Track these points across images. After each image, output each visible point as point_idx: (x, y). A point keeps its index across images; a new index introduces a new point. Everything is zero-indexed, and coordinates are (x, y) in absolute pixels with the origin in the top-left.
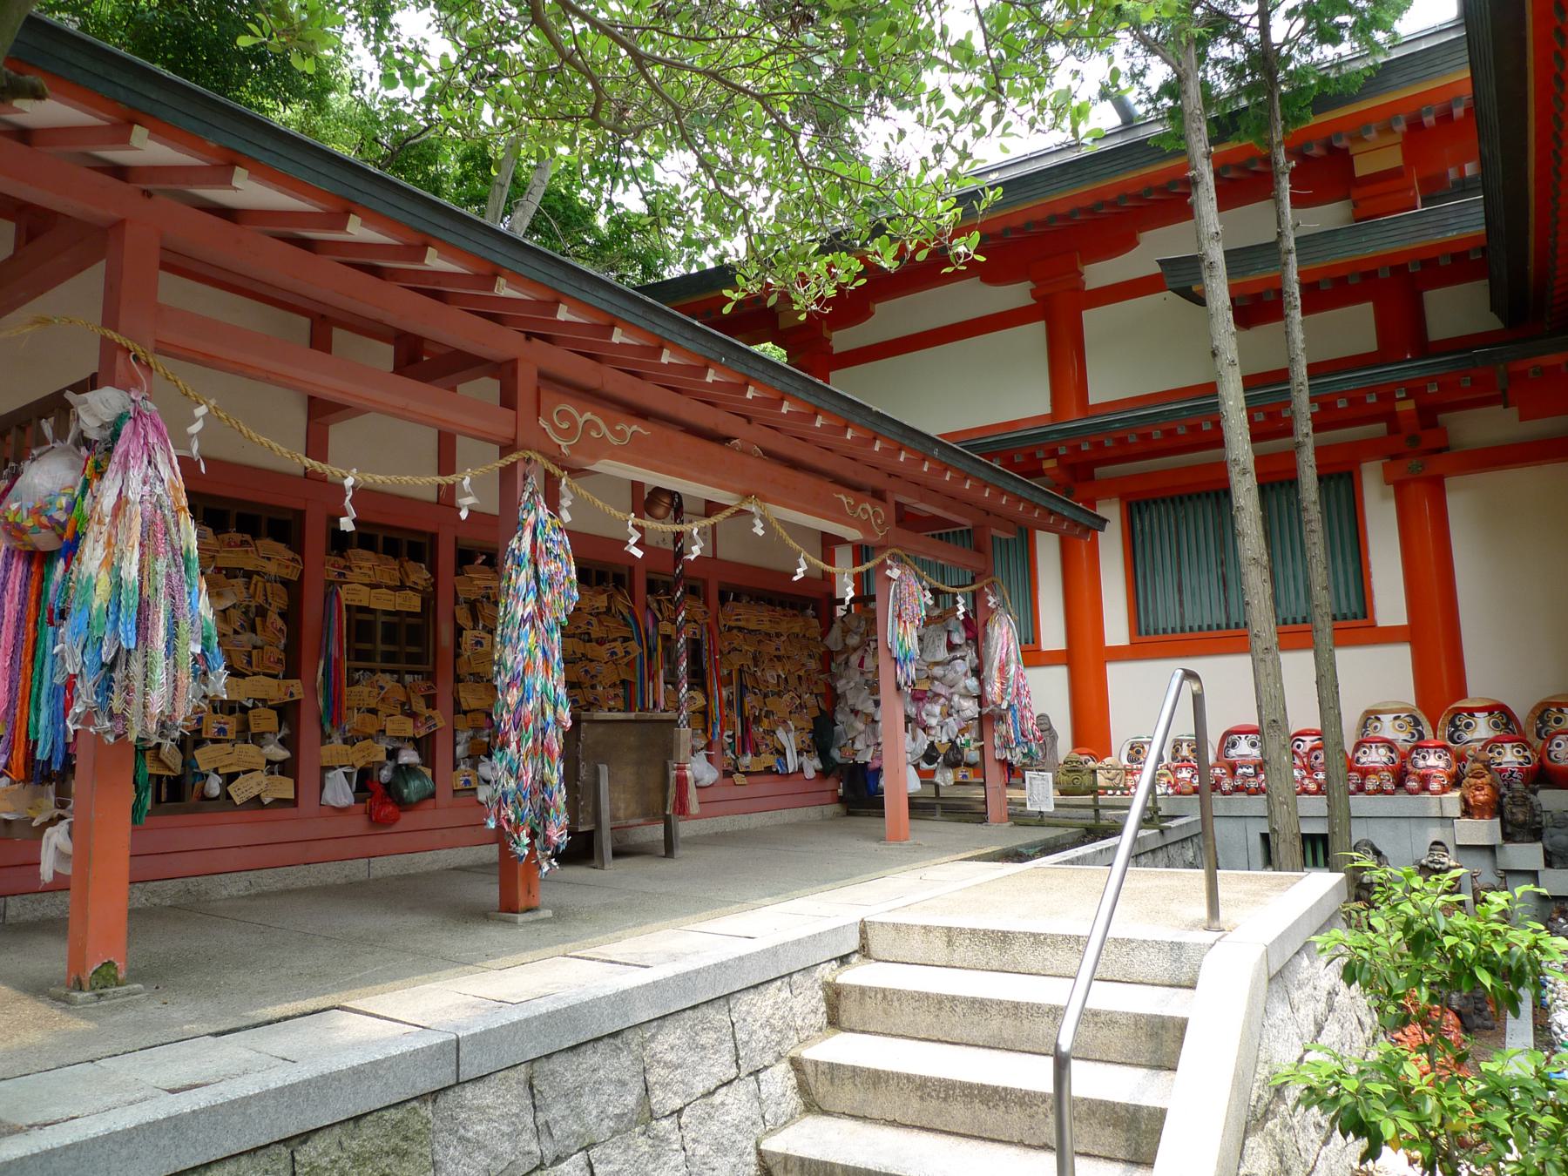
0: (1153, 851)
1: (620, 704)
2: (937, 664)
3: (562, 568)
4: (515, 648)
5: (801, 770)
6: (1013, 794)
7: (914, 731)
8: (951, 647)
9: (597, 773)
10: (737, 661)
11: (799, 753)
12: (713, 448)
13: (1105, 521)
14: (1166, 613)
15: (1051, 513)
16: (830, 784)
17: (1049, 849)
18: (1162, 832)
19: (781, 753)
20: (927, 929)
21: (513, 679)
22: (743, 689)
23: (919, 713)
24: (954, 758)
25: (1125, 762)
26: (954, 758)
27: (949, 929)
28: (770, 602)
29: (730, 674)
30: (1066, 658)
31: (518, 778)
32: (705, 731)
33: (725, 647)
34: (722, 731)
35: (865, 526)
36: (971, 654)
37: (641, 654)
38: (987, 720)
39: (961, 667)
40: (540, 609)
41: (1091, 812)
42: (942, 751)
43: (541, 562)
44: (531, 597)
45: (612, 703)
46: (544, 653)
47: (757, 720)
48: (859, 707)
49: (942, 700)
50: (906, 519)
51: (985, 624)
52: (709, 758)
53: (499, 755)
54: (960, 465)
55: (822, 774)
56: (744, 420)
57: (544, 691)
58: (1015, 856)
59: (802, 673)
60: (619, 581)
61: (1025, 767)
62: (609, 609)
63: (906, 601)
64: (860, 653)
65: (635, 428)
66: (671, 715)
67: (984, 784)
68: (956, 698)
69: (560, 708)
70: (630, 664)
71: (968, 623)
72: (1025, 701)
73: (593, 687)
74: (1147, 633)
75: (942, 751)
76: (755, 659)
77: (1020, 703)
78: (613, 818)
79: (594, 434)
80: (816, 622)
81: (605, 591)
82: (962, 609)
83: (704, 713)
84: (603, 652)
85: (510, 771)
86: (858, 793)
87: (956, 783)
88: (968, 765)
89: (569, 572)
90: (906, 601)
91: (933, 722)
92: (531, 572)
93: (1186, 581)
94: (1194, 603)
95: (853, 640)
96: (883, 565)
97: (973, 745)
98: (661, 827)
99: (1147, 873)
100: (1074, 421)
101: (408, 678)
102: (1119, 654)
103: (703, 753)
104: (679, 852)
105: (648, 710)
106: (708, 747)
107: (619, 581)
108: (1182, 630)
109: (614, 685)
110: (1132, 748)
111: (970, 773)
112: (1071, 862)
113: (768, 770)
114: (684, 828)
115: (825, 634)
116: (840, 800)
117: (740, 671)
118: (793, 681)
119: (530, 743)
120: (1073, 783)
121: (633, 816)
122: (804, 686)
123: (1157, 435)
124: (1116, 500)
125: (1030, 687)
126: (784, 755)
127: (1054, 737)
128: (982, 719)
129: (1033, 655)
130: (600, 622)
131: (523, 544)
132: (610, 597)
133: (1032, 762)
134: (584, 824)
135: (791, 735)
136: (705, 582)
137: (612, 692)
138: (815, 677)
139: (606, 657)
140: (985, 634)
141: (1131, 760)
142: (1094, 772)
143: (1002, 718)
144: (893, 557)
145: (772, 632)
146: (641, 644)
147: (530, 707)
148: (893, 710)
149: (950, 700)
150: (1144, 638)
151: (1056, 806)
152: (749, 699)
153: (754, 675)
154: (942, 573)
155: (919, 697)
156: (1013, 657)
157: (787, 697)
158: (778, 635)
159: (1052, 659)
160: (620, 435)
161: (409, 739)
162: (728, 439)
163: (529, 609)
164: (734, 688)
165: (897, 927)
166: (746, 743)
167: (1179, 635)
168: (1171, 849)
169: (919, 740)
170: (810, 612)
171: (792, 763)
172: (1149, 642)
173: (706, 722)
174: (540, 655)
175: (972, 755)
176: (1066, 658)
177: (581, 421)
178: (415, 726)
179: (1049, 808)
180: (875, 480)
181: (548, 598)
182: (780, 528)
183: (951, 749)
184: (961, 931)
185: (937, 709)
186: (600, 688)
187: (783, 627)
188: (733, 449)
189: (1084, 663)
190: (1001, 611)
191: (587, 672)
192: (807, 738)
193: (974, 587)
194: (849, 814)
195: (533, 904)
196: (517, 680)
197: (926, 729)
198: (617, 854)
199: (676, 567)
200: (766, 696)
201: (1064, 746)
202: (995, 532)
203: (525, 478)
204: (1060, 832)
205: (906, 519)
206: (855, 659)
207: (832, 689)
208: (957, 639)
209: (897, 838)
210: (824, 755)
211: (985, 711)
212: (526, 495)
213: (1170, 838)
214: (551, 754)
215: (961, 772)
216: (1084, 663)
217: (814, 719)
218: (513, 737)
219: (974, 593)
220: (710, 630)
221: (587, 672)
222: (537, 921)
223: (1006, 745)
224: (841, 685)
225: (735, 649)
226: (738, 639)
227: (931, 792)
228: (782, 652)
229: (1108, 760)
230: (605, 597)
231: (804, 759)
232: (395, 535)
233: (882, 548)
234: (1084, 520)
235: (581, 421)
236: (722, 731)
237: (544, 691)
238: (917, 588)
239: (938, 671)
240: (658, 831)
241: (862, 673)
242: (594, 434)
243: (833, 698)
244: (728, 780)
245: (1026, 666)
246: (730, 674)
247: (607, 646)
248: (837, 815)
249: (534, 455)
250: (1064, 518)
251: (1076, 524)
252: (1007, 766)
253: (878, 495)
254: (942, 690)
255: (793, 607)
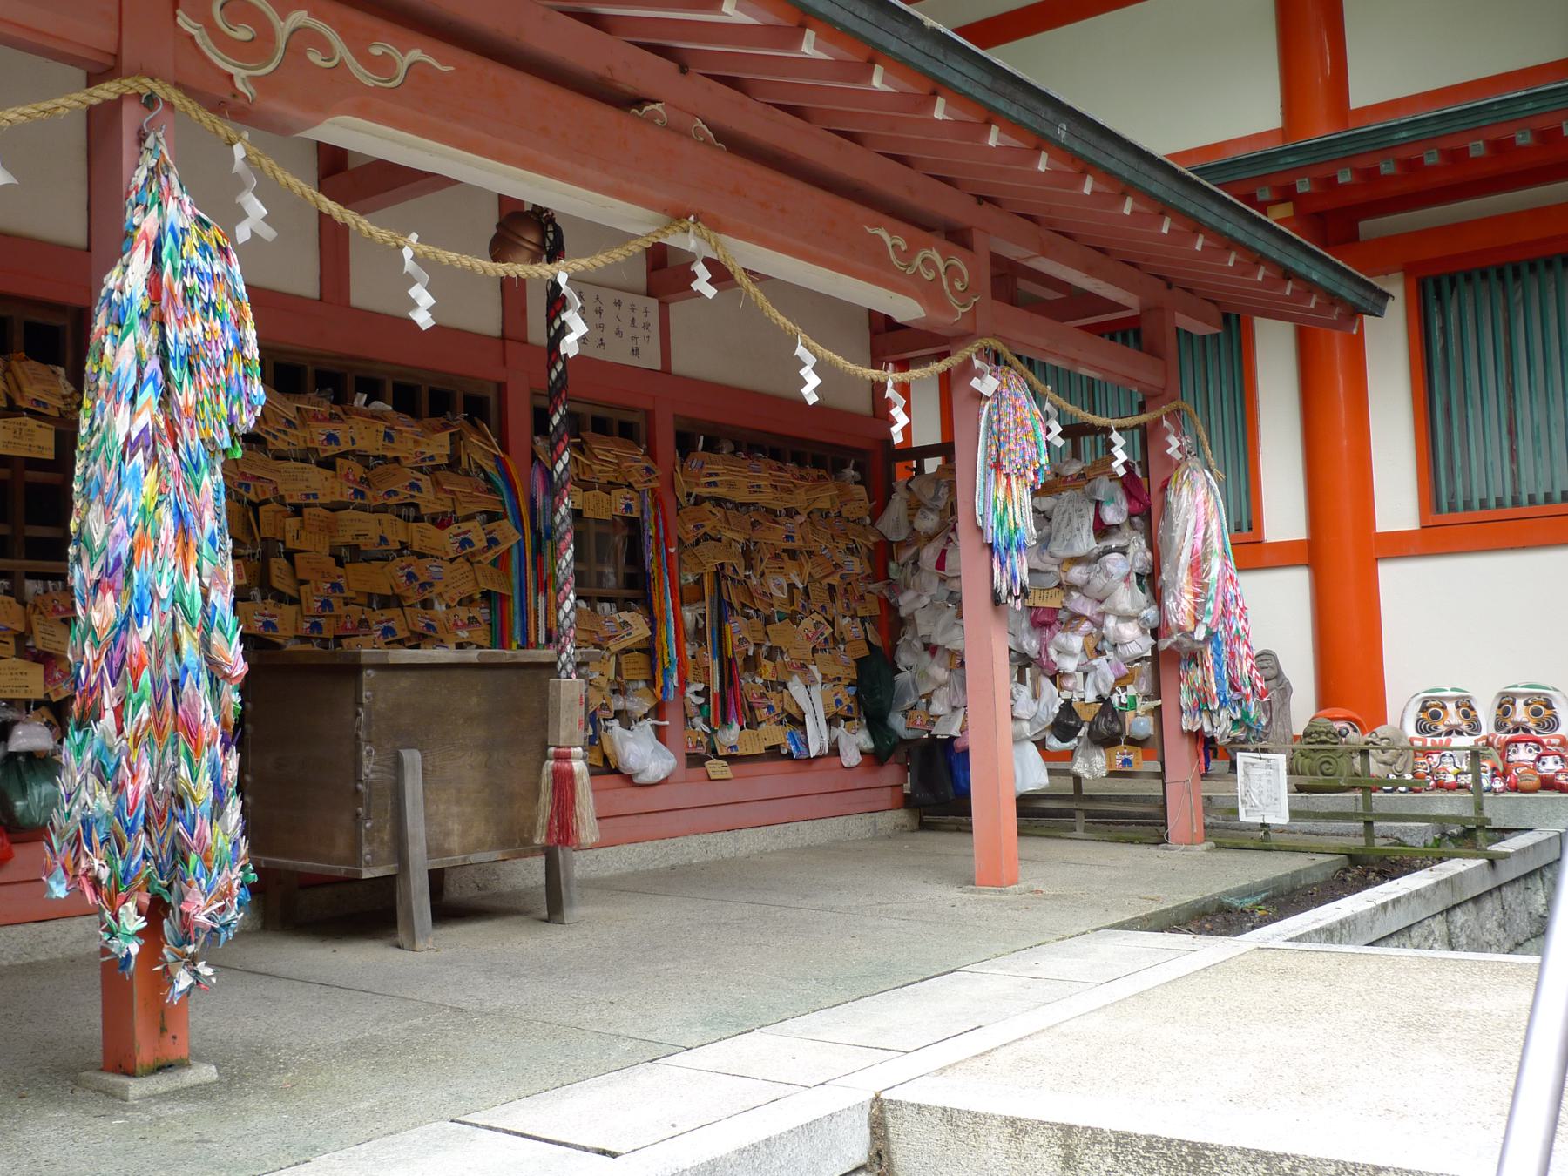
0: (1476, 899)
1: (480, 634)
2: (1076, 561)
3: (228, 339)
4: (108, 507)
5: (835, 750)
6: (1213, 789)
7: (1034, 680)
8: (1102, 530)
9: (398, 765)
10: (710, 557)
11: (831, 721)
12: (604, 115)
13: (1385, 296)
14: (1485, 473)
15: (1288, 274)
16: (890, 774)
17: (1286, 899)
18: (1492, 863)
19: (797, 721)
20: (1017, 1127)
21: (108, 572)
22: (723, 610)
23: (1043, 650)
24: (1107, 730)
25: (1410, 731)
26: (1107, 730)
27: (1068, 1130)
28: (775, 454)
29: (699, 582)
30: (1308, 555)
31: (119, 788)
32: (651, 683)
33: (688, 531)
34: (684, 683)
35: (928, 293)
36: (1139, 554)
37: (521, 544)
38: (1168, 658)
39: (1116, 564)
40: (170, 423)
41: (1359, 826)
42: (1086, 716)
43: (171, 319)
44: (148, 396)
45: (463, 634)
46: (180, 516)
47: (752, 663)
48: (938, 640)
49: (1086, 626)
50: (1006, 280)
51: (1164, 487)
52: (660, 734)
53: (77, 737)
54: (1111, 164)
55: (873, 759)
56: (669, 66)
57: (177, 600)
58: (1217, 917)
59: (835, 580)
60: (477, 409)
61: (1237, 744)
62: (454, 463)
63: (1008, 446)
64: (938, 544)
65: (416, 54)
66: (545, 655)
67: (1161, 775)
68: (1111, 622)
69: (216, 638)
70: (501, 562)
71: (1131, 486)
72: (1237, 625)
73: (427, 604)
74: (1452, 508)
75: (1086, 716)
76: (748, 557)
77: (1228, 628)
78: (434, 850)
79: (315, 57)
80: (861, 491)
81: (445, 427)
82: (1121, 456)
83: (649, 650)
84: (446, 540)
85: (101, 772)
86: (933, 787)
87: (1112, 774)
88: (1132, 742)
89: (241, 343)
90: (1008, 446)
91: (1069, 665)
92: (150, 342)
93: (1523, 414)
94: (1537, 453)
95: (928, 522)
96: (967, 370)
97: (1143, 706)
98: (539, 863)
99: (1497, 969)
100: (1322, 131)
101: (32, 587)
102: (1401, 546)
103: (647, 724)
104: (573, 913)
105: (536, 645)
106: (658, 711)
107: (477, 409)
108: (1516, 502)
109: (468, 601)
110: (1424, 709)
111: (1135, 756)
112: (1329, 934)
113: (774, 753)
114: (580, 866)
115: (878, 511)
116: (907, 802)
117: (718, 577)
118: (819, 595)
119: (144, 713)
120: (1316, 768)
121: (479, 846)
122: (840, 604)
123: (1477, 149)
124: (1399, 276)
125: (1247, 600)
126: (803, 724)
127: (1285, 691)
128: (1158, 660)
129: (1251, 550)
130: (437, 484)
131: (130, 278)
132: (456, 439)
133: (1253, 736)
134: (374, 863)
135: (816, 691)
136: (649, 415)
137: (463, 614)
138: (861, 587)
139: (452, 549)
140: (1165, 504)
141: (1422, 728)
142: (1364, 753)
143: (1194, 657)
144: (984, 353)
145: (779, 506)
146: (519, 526)
147: (145, 633)
148: (989, 643)
149: (1100, 626)
150: (1446, 517)
151: (1295, 815)
152: (736, 627)
153: (744, 583)
154: (1090, 393)
155: (1043, 621)
156: (1216, 545)
157: (807, 623)
158: (791, 513)
159: (1283, 556)
160: (382, 66)
161: (38, 704)
162: (640, 102)
163: (144, 420)
164: (707, 607)
165: (950, 1117)
166: (728, 703)
167: (1509, 511)
168: (1508, 893)
169: (1045, 697)
170: (850, 472)
171: (817, 738)
172: (1452, 526)
173: (653, 668)
174: (168, 519)
175: (1140, 724)
176: (1308, 555)
177: (283, 28)
178: (48, 676)
179: (1279, 816)
180: (953, 207)
181: (186, 396)
182: (792, 313)
183: (1102, 712)
184: (1095, 1136)
185: (1076, 642)
186: (440, 607)
187: (799, 499)
188: (650, 119)
189: (1339, 561)
190: (1193, 462)
191: (411, 576)
192: (846, 695)
193: (1143, 418)
194: (924, 826)
195: (175, 1052)
196: (118, 573)
197: (1056, 677)
198: (447, 912)
199: (551, 366)
200: (768, 621)
201: (1302, 708)
202: (1184, 322)
203: (141, 138)
204: (1298, 863)
205: (1006, 280)
206: (929, 555)
207: (890, 608)
208: (1111, 516)
209: (996, 879)
210: (877, 724)
211: (1165, 644)
212: (141, 175)
213: (1507, 872)
214: (191, 731)
215: (1119, 754)
216: (1339, 561)
217: (860, 662)
218: (109, 699)
219: (1143, 429)
220: (658, 502)
221: (411, 576)
222: (163, 1097)
223: (1202, 705)
224: (907, 602)
225: (707, 537)
226: (713, 520)
227: (1067, 785)
228: (798, 544)
229: (1381, 731)
230: (444, 437)
231: (841, 731)
232: (53, 320)
233: (964, 338)
234: (1347, 292)
235: (283, 28)
236: (684, 683)
237: (177, 600)
238: (1031, 412)
239: (1077, 574)
240: (532, 872)
241: (943, 580)
242: (315, 57)
243: (893, 623)
244: (696, 772)
245: (1240, 569)
246: (699, 582)
247: (453, 529)
248: (901, 830)
249: (163, 91)
250: (1309, 286)
251: (1332, 299)
252: (1206, 745)
253: (958, 236)
254: (1087, 608)
255: (818, 463)
